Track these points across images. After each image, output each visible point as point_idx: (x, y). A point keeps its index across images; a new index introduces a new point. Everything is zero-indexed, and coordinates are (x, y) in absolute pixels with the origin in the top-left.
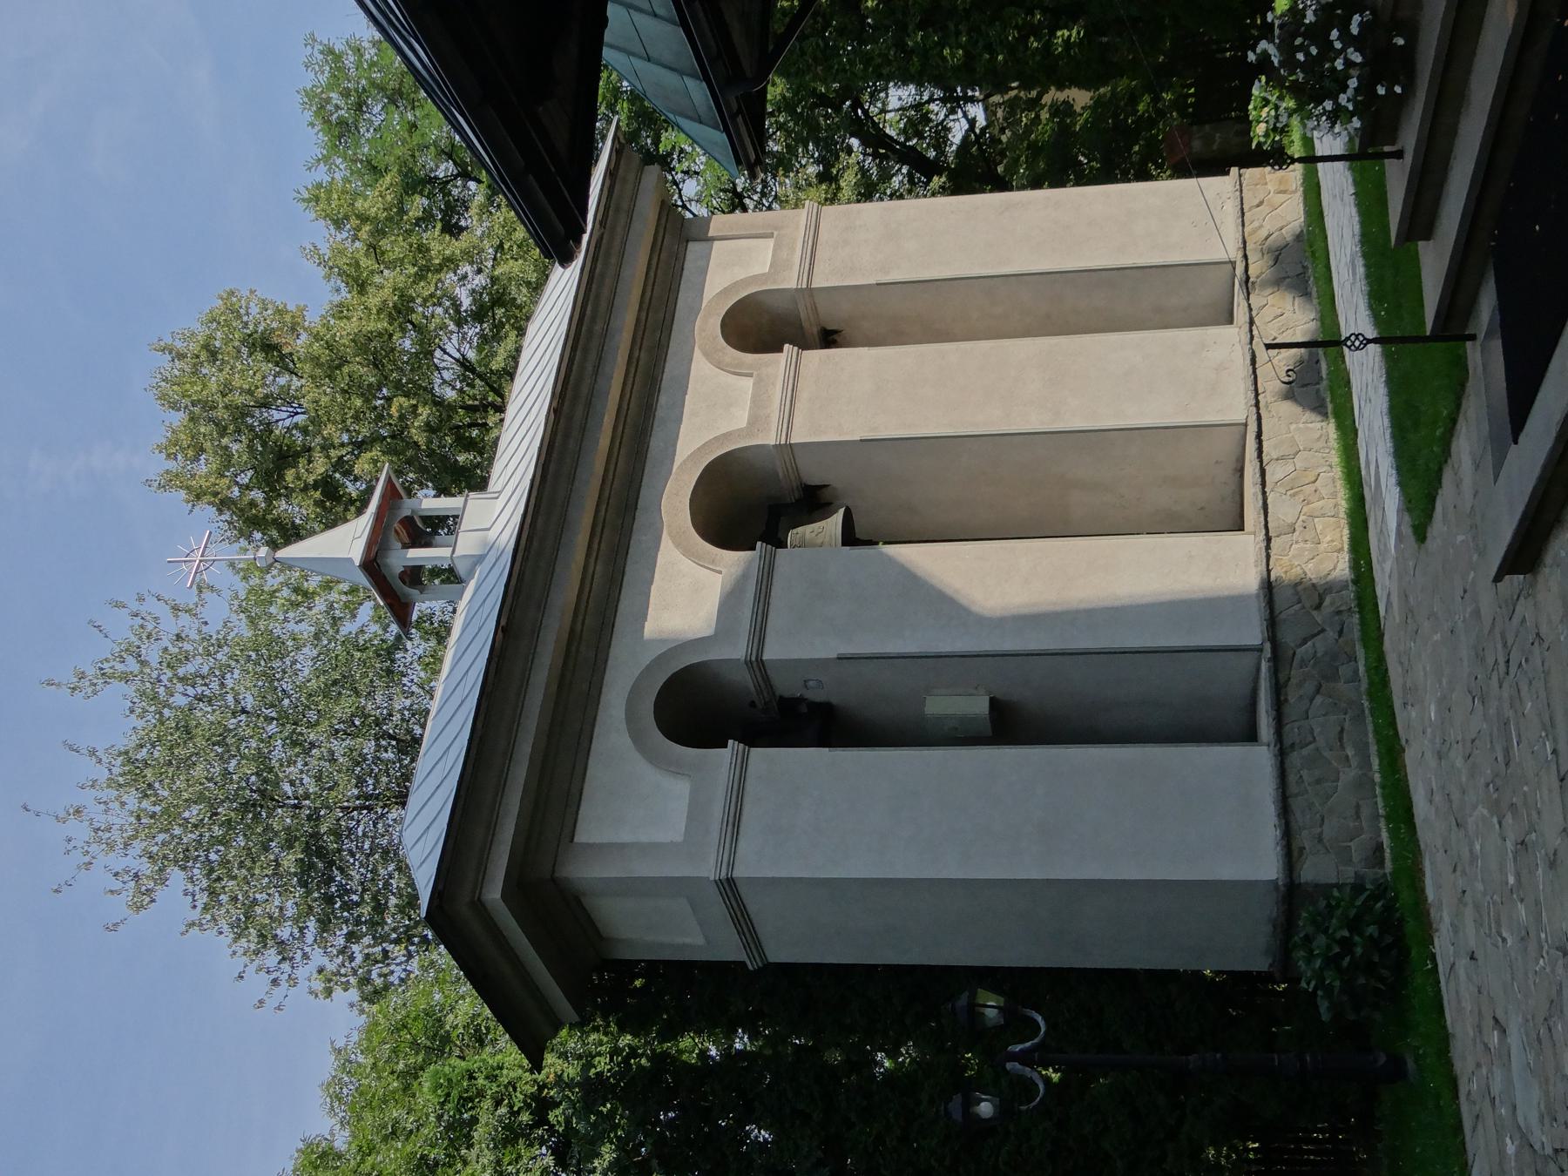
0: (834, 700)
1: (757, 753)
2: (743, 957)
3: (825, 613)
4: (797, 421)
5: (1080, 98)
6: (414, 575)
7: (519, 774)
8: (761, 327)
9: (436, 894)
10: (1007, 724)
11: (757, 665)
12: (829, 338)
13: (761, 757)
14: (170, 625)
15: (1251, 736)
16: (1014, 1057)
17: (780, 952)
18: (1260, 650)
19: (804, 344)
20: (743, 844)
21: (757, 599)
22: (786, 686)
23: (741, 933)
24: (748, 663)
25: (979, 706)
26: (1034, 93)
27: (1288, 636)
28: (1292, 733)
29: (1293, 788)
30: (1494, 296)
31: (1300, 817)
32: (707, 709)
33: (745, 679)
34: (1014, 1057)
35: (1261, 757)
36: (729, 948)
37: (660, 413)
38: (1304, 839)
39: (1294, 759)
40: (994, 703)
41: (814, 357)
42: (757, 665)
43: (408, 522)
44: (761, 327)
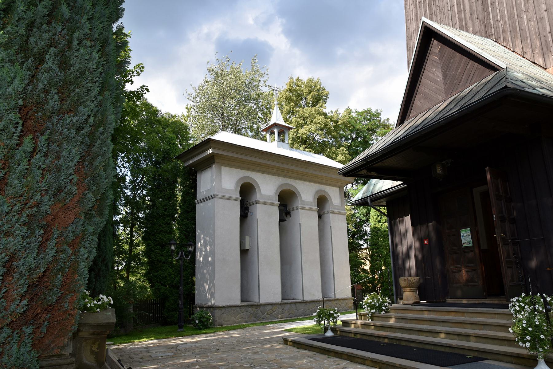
0: (248, 218)
1: (239, 203)
2: (197, 199)
3: (266, 217)
4: (304, 211)
5: (367, 268)
6: (273, 133)
7: (236, 155)
8: (322, 201)
9: (213, 140)
10: (244, 252)
11: (298, 208)
12: (320, 217)
13: (238, 204)
14: (262, 79)
15: (242, 301)
16: (182, 253)
17: (199, 207)
18: (259, 302)
19: (242, 202)
20: (221, 200)
21: (268, 203)
22: (251, 208)
23: (203, 199)
24: (256, 201)
25: (247, 247)
26: (369, 258)
27: (262, 308)
28: (243, 308)
29: (233, 308)
30: (299, 182)
31: (228, 309)
32: (246, 191)
33: (253, 200)
34: (182, 253)
35: (238, 302)
36: (199, 196)
37: (305, 182)
38: (223, 311)
39: (238, 309)
40: (248, 250)
41: (316, 214)
42: (298, 208)
43: (283, 131)
44: (322, 201)
